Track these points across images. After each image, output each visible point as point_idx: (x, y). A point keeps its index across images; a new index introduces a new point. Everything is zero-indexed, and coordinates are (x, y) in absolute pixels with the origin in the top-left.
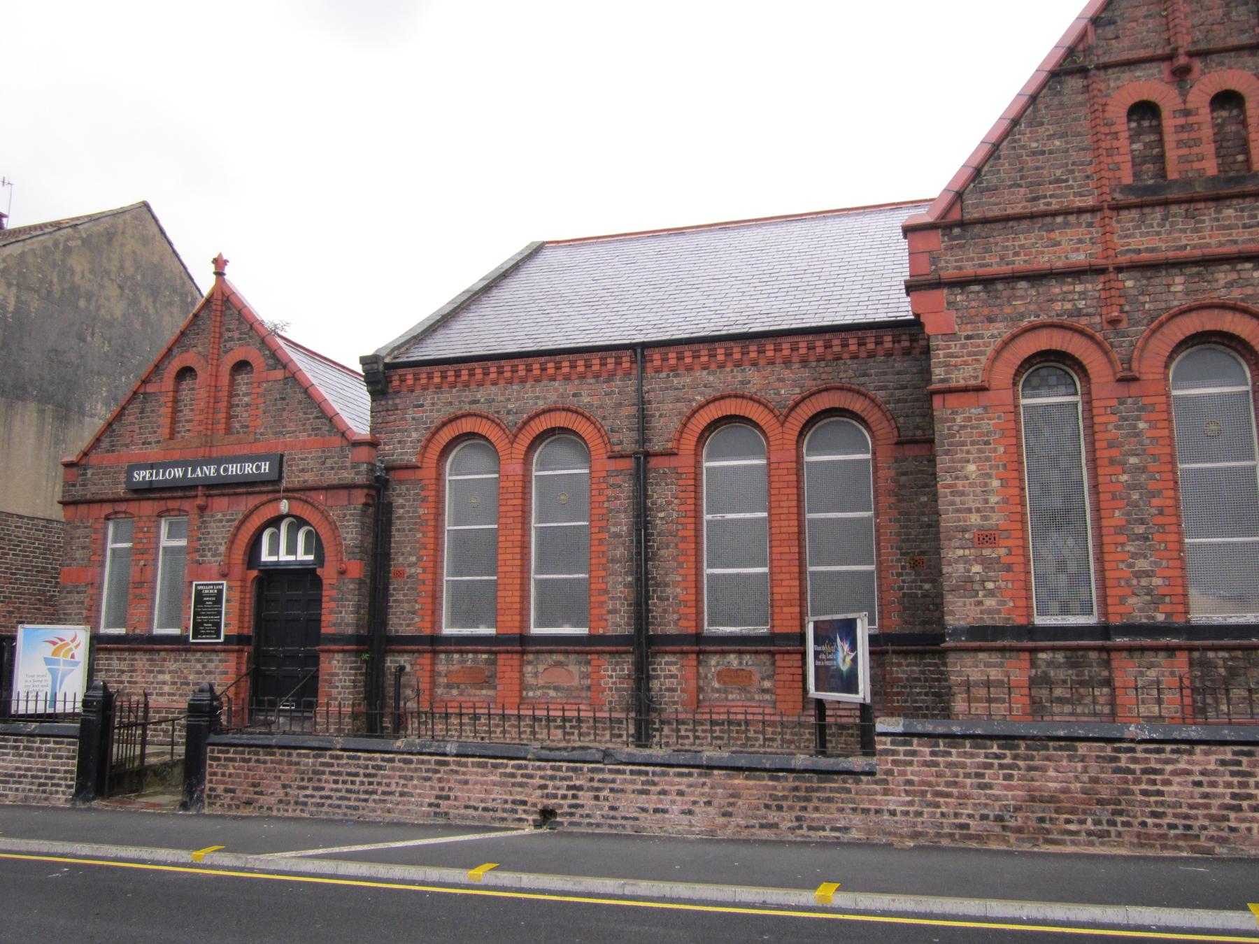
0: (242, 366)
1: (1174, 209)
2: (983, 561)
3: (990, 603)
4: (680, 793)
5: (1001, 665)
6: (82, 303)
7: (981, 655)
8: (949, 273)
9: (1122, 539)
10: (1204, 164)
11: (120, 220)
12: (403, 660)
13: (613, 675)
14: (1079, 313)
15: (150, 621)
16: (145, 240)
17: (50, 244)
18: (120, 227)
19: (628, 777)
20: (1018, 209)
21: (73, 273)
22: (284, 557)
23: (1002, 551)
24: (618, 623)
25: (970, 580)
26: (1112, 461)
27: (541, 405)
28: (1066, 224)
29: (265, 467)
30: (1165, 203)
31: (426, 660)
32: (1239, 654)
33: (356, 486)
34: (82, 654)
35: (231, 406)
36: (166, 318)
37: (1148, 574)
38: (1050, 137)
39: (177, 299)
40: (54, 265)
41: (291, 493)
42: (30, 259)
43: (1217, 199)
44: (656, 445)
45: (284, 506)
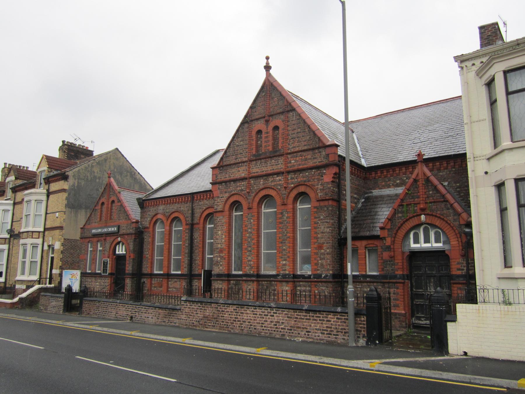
1: (263, 161)
2: (220, 256)
3: (221, 268)
5: (222, 284)
6: (97, 180)
7: (219, 281)
9: (246, 251)
11: (109, 155)
12: (145, 280)
15: (95, 269)
16: (117, 159)
17: (87, 166)
18: (109, 157)
19: (305, 320)
20: (232, 162)
21: (94, 172)
22: (121, 253)
23: (224, 254)
24: (185, 271)
25: (217, 262)
27: (173, 210)
28: (242, 166)
29: (116, 229)
30: (260, 159)
31: (149, 280)
32: (269, 282)
33: (132, 234)
34: (79, 277)
35: (111, 212)
36: (125, 180)
38: (241, 141)
39: (129, 174)
40: (88, 171)
41: (122, 235)
42: (81, 171)
43: (270, 157)
44: (195, 222)
45: (119, 239)
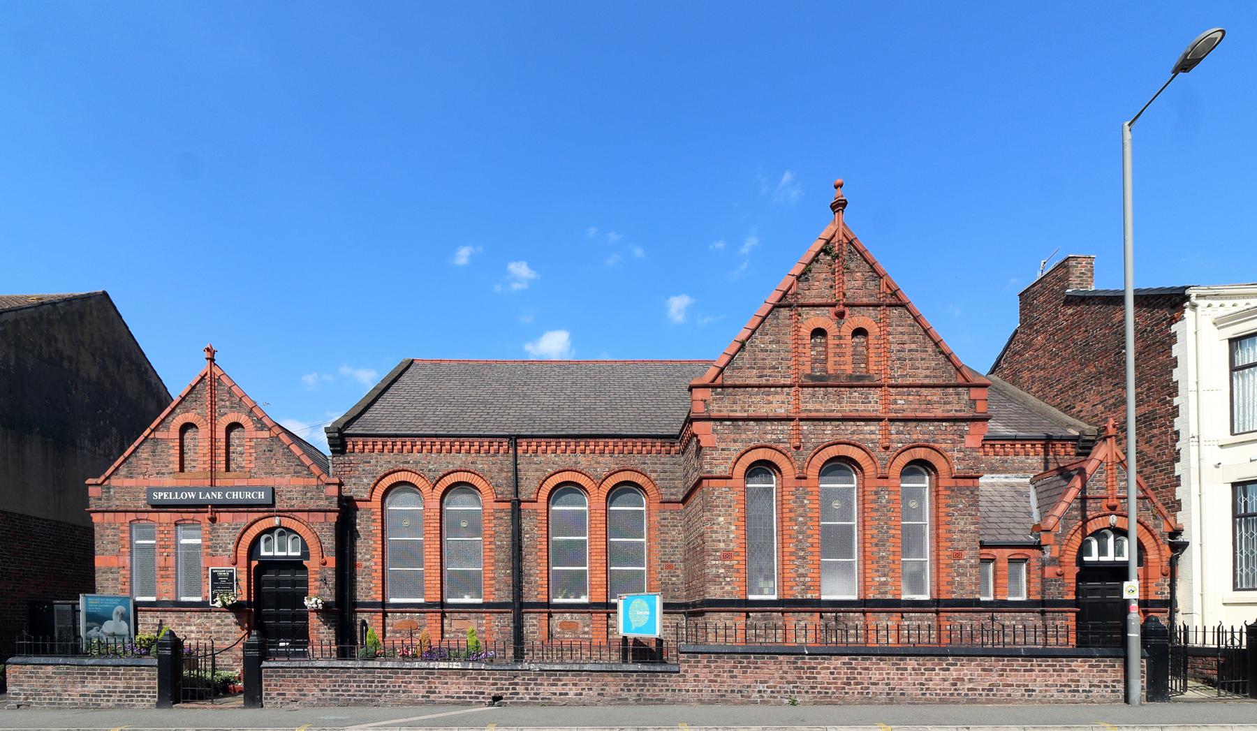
0: (233, 426)
2: (726, 567)
3: (728, 588)
4: (575, 685)
6: (66, 364)
8: (714, 414)
10: (846, 367)
12: (364, 616)
13: (499, 625)
14: (779, 441)
26: (791, 519)
27: (451, 468)
28: (776, 393)
37: (804, 576)
38: (771, 342)
